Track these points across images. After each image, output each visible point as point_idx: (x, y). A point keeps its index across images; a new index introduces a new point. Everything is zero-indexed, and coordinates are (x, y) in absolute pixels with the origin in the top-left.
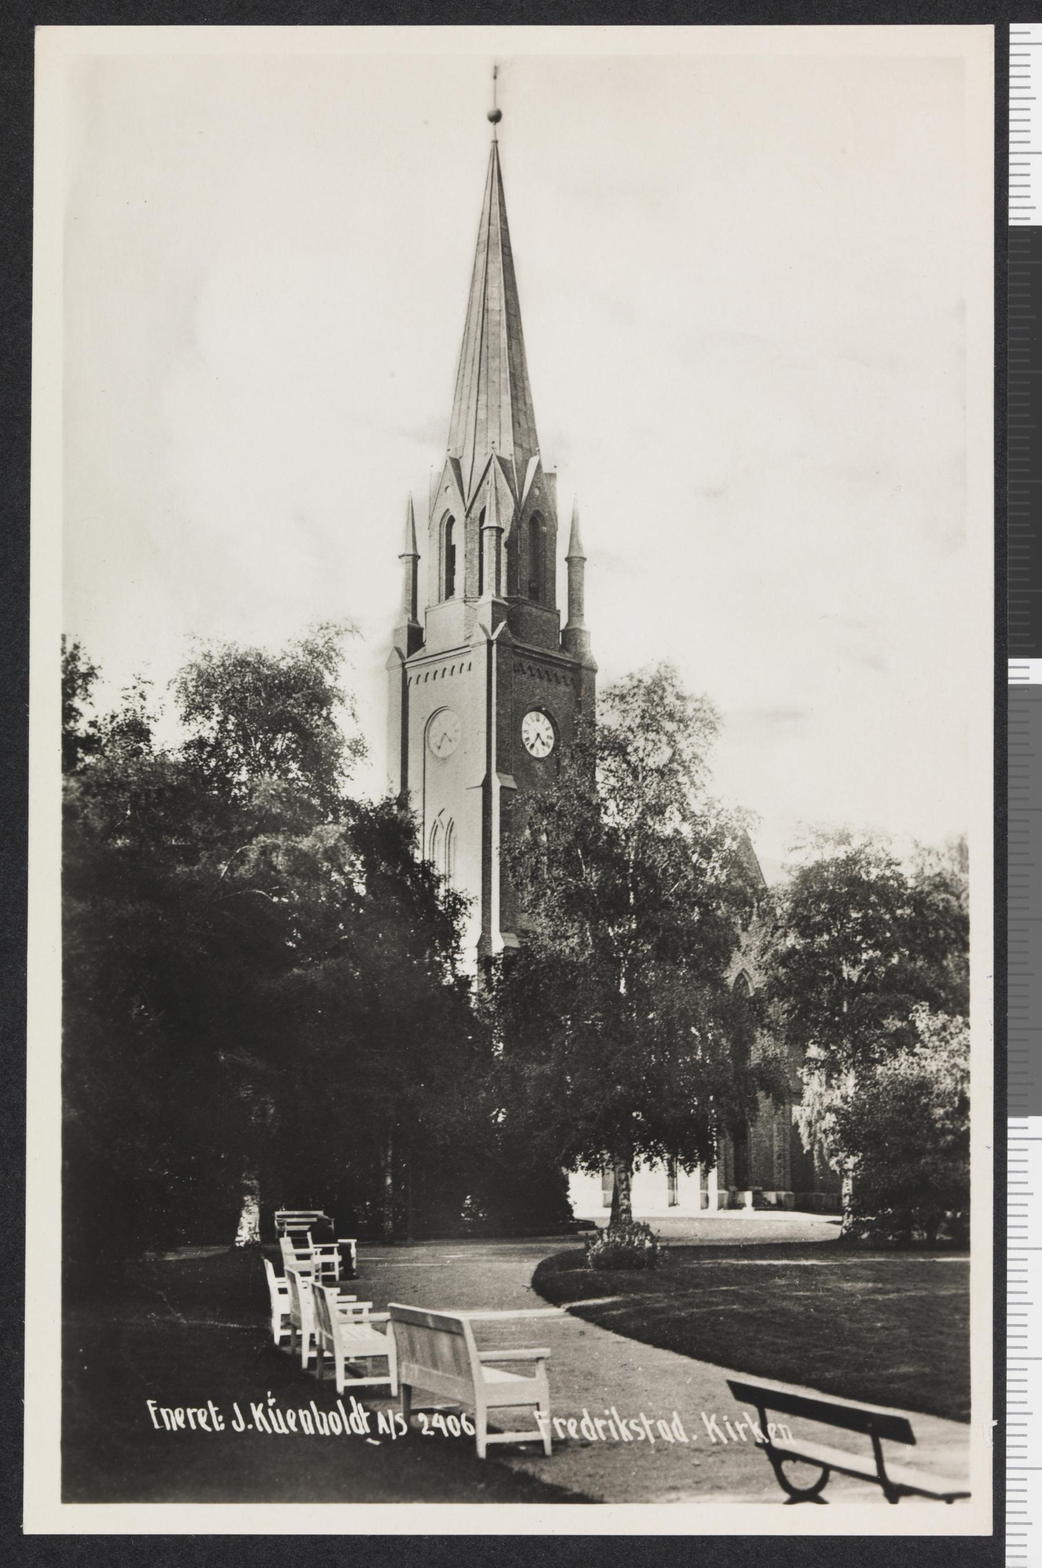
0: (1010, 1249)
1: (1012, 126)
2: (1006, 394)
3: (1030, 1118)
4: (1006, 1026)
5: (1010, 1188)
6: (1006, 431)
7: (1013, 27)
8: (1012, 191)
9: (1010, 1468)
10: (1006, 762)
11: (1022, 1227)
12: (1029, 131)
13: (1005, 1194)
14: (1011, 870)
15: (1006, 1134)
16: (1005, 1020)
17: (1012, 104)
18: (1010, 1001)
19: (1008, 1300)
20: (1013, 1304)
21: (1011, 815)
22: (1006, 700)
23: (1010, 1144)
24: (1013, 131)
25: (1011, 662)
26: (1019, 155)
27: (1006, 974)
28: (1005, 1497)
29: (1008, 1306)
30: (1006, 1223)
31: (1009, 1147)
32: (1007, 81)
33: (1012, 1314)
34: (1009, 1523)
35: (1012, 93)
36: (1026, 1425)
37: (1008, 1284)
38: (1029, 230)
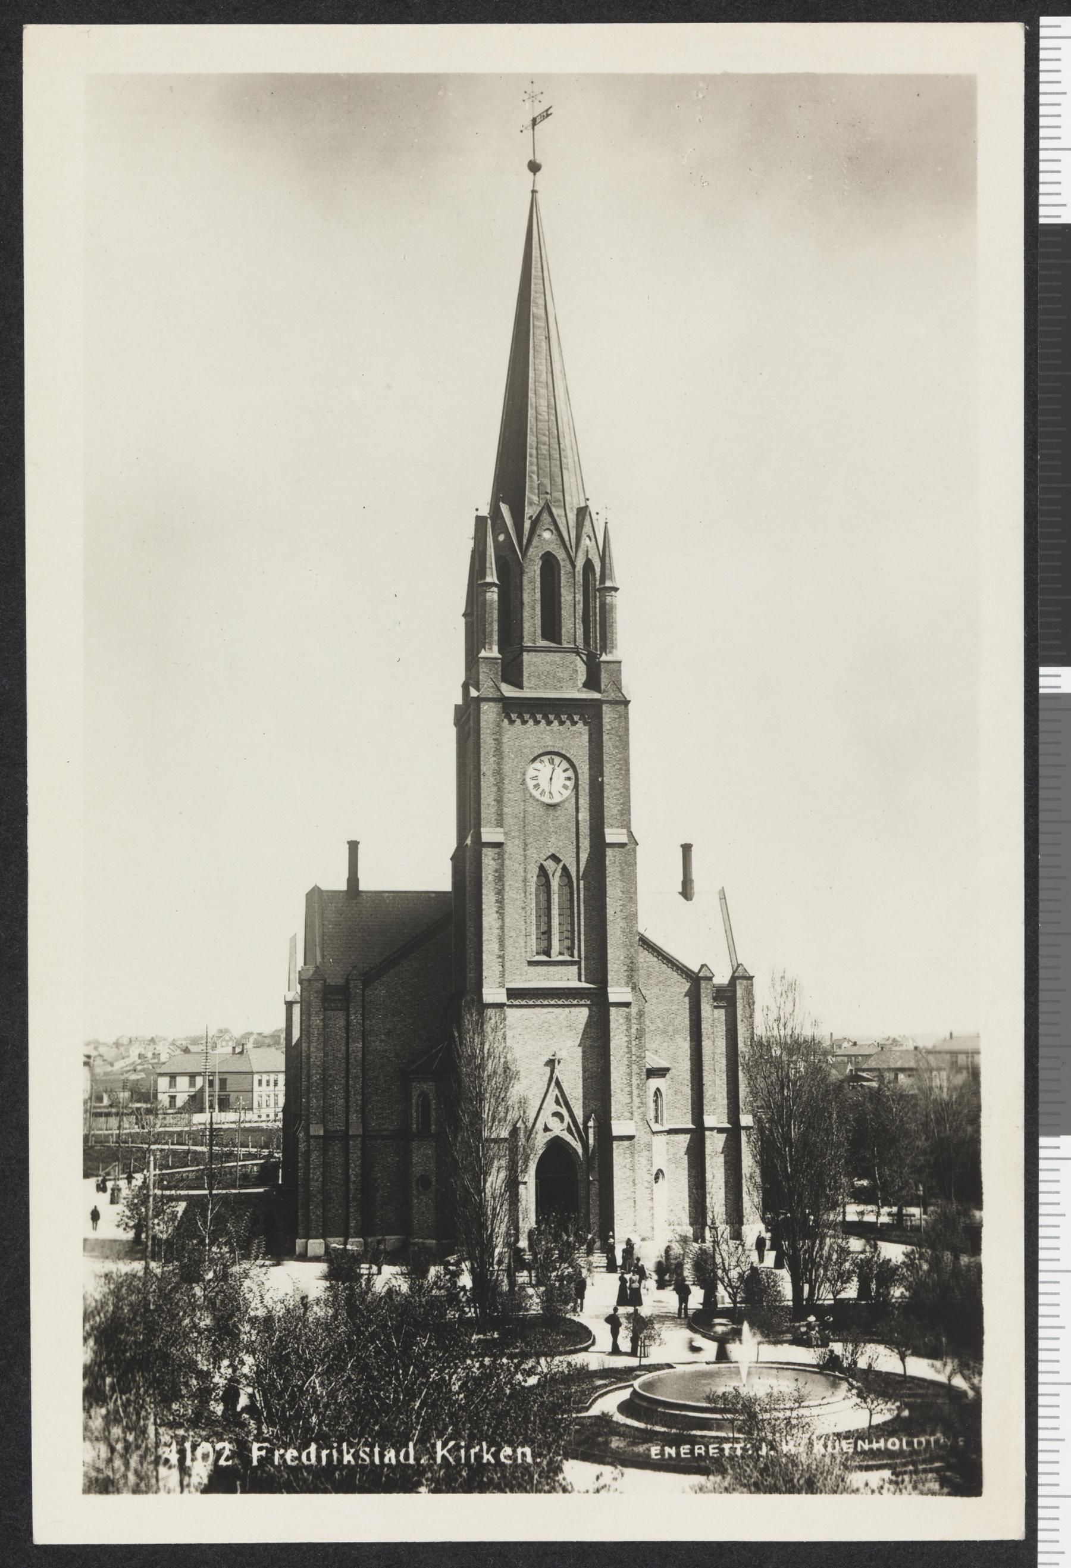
0: (1042, 1271)
1: (1042, 121)
2: (1036, 397)
3: (1062, 1137)
4: (1038, 1043)
5: (1042, 1210)
6: (1036, 434)
7: (1044, 20)
8: (1042, 189)
9: (1042, 1440)
10: (1037, 773)
11: (1054, 1249)
12: (1060, 127)
13: (1037, 1215)
14: (1042, 883)
15: (1037, 1154)
16: (1037, 1037)
17: (1042, 99)
18: (1042, 1018)
19: (1040, 1324)
20: (1046, 105)
21: (1042, 827)
22: (1037, 710)
23: (1042, 1164)
24: (1043, 127)
25: (1043, 670)
26: (1049, 152)
27: (1038, 990)
28: (1037, 1525)
29: (1040, 1398)
30: (1038, 1245)
31: (1040, 1167)
32: (1037, 76)
33: (1044, 205)
34: (1041, 1552)
35: (1043, 88)
36: (1058, 1541)
37: (1040, 1308)
38: (1059, 228)
